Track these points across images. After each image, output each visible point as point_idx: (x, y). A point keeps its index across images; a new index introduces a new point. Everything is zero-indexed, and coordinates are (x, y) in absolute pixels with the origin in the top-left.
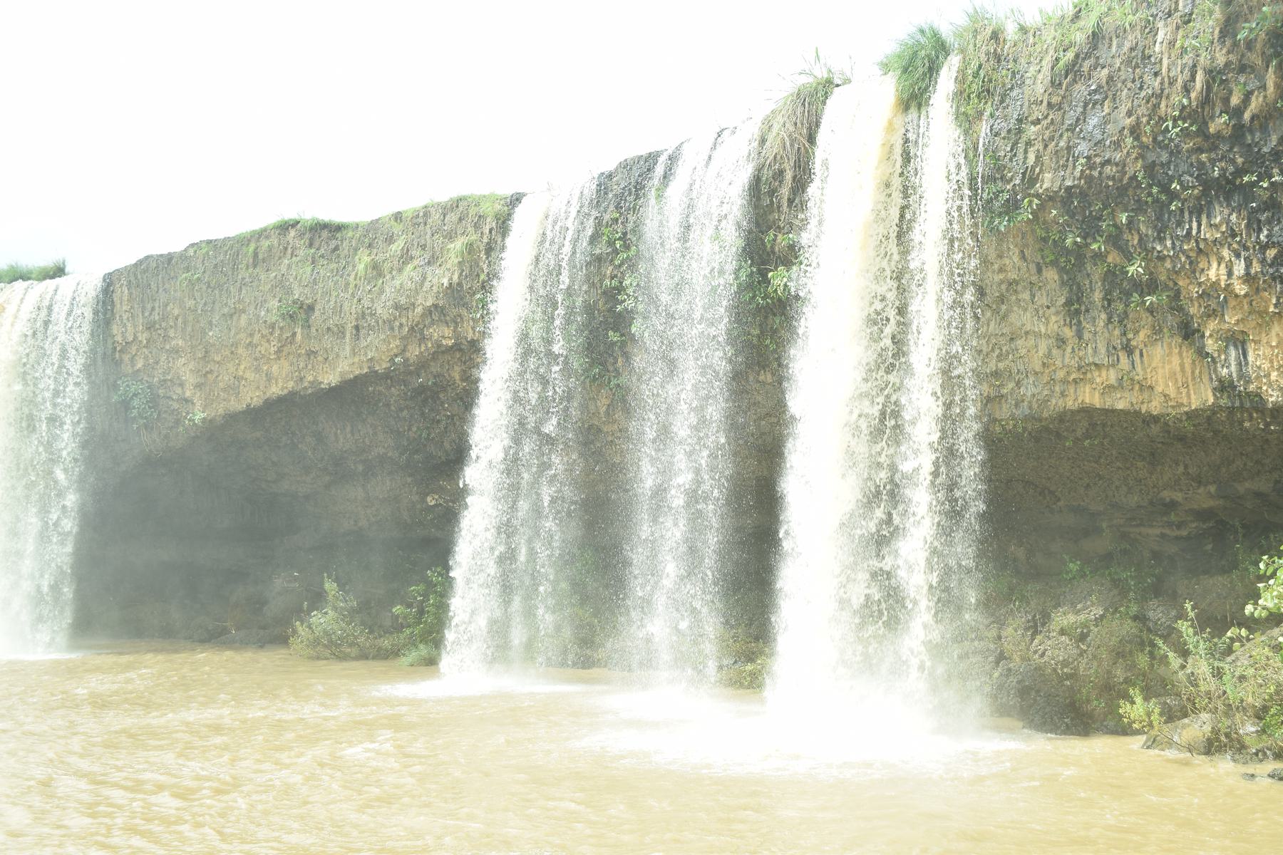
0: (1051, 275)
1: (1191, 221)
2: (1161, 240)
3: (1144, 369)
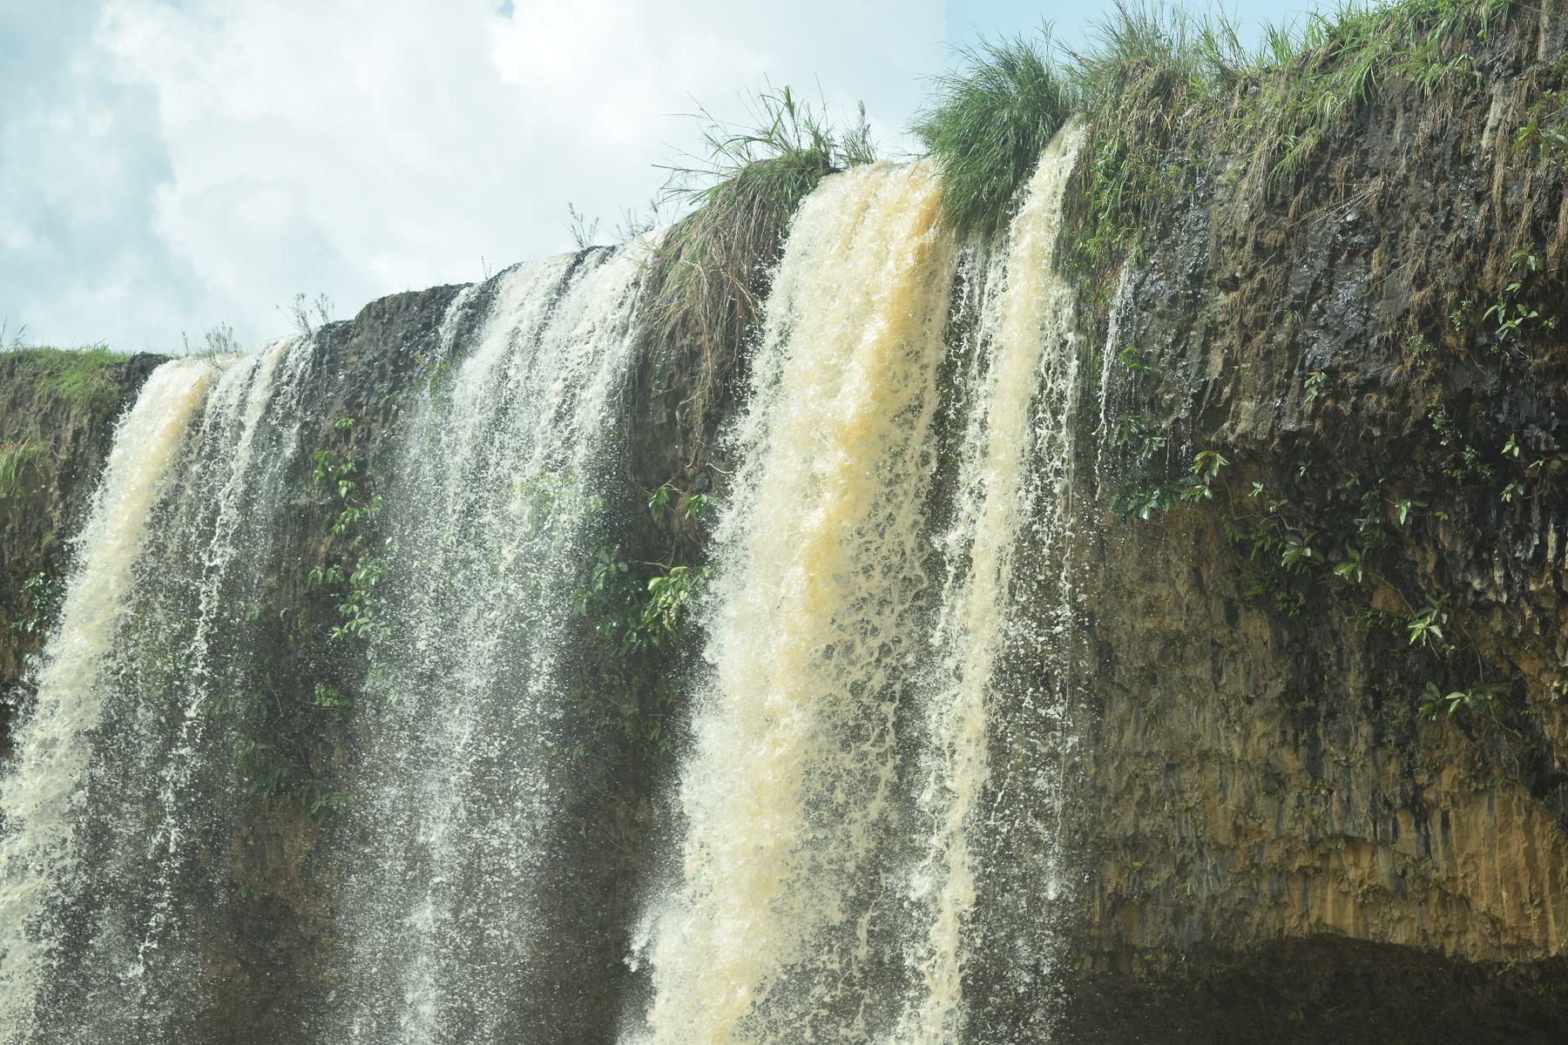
0: (1256, 627)
1: (1544, 531)
2: (1484, 568)
3: (1450, 857)
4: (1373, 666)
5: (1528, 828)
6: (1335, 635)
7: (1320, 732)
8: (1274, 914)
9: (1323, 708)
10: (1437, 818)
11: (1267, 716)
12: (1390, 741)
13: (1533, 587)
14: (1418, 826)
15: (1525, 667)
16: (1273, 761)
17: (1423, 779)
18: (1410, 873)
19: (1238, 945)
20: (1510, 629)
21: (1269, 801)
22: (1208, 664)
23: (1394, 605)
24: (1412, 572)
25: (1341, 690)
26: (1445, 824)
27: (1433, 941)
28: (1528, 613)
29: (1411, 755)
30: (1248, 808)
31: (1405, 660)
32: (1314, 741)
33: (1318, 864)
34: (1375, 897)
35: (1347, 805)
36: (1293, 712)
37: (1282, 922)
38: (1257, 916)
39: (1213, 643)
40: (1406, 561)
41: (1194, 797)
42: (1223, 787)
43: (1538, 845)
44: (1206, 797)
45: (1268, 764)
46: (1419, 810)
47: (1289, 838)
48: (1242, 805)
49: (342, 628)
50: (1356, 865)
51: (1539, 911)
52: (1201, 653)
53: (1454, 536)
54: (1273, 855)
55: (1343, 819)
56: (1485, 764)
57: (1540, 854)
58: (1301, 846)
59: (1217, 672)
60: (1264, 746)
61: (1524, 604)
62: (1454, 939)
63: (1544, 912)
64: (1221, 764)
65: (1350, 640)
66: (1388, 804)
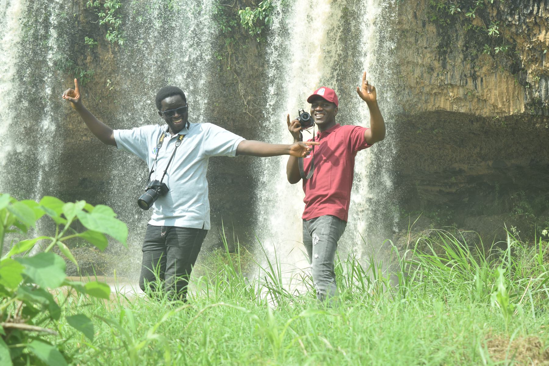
0: (432, 29)
1: (533, 6)
2: (512, 15)
3: (483, 90)
4: (467, 39)
5: (507, 82)
6: (456, 31)
7: (447, 57)
8: (425, 105)
9: (449, 50)
10: (479, 79)
11: (432, 52)
12: (469, 59)
13: (527, 21)
14: (473, 81)
15: (518, 41)
16: (431, 64)
17: (477, 69)
18: (469, 94)
19: (413, 113)
20: (517, 31)
21: (428, 75)
22: (414, 38)
23: (480, 24)
24: (488, 15)
25: (456, 45)
26: (482, 81)
27: (472, 111)
28: (524, 27)
29: (475, 63)
30: (421, 77)
31: (478, 38)
32: (445, 58)
33: (440, 92)
34: (458, 100)
35: (452, 76)
36: (440, 51)
37: (427, 107)
38: (420, 106)
39: (417, 32)
40: (487, 12)
41: (405, 74)
42: (413, 71)
43: (509, 86)
44: (408, 74)
45: (430, 65)
46: (474, 77)
47: (433, 85)
48: (420, 76)
49: (103, 20)
50: (452, 92)
51: (508, 103)
52: (412, 35)
53: (505, 6)
54: (427, 89)
55: (451, 80)
56: (497, 65)
57: (510, 89)
58: (436, 87)
59: (417, 41)
60: (429, 60)
61: (523, 25)
62: (479, 111)
63: (510, 103)
64: (413, 65)
65: (461, 33)
66: (465, 76)
